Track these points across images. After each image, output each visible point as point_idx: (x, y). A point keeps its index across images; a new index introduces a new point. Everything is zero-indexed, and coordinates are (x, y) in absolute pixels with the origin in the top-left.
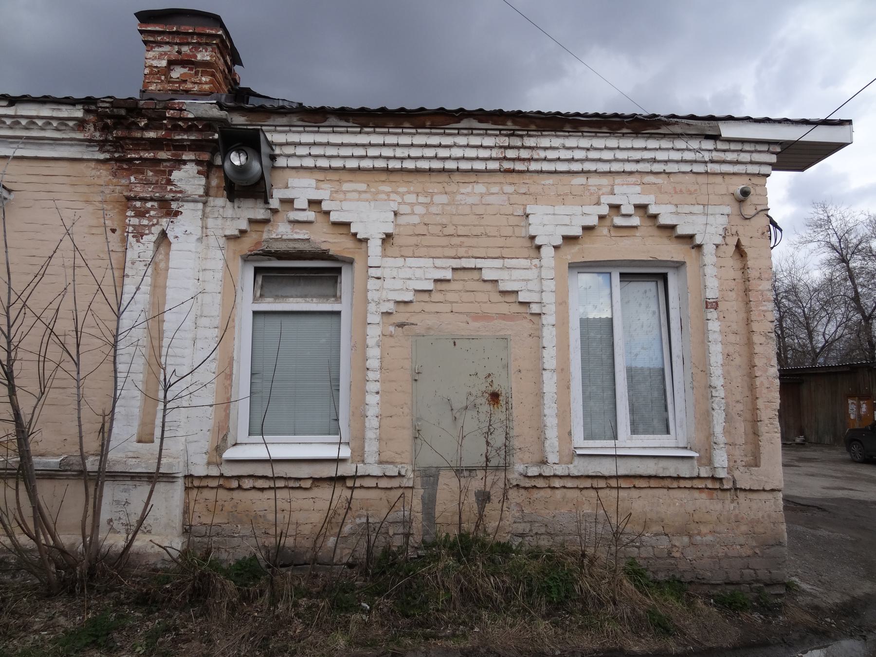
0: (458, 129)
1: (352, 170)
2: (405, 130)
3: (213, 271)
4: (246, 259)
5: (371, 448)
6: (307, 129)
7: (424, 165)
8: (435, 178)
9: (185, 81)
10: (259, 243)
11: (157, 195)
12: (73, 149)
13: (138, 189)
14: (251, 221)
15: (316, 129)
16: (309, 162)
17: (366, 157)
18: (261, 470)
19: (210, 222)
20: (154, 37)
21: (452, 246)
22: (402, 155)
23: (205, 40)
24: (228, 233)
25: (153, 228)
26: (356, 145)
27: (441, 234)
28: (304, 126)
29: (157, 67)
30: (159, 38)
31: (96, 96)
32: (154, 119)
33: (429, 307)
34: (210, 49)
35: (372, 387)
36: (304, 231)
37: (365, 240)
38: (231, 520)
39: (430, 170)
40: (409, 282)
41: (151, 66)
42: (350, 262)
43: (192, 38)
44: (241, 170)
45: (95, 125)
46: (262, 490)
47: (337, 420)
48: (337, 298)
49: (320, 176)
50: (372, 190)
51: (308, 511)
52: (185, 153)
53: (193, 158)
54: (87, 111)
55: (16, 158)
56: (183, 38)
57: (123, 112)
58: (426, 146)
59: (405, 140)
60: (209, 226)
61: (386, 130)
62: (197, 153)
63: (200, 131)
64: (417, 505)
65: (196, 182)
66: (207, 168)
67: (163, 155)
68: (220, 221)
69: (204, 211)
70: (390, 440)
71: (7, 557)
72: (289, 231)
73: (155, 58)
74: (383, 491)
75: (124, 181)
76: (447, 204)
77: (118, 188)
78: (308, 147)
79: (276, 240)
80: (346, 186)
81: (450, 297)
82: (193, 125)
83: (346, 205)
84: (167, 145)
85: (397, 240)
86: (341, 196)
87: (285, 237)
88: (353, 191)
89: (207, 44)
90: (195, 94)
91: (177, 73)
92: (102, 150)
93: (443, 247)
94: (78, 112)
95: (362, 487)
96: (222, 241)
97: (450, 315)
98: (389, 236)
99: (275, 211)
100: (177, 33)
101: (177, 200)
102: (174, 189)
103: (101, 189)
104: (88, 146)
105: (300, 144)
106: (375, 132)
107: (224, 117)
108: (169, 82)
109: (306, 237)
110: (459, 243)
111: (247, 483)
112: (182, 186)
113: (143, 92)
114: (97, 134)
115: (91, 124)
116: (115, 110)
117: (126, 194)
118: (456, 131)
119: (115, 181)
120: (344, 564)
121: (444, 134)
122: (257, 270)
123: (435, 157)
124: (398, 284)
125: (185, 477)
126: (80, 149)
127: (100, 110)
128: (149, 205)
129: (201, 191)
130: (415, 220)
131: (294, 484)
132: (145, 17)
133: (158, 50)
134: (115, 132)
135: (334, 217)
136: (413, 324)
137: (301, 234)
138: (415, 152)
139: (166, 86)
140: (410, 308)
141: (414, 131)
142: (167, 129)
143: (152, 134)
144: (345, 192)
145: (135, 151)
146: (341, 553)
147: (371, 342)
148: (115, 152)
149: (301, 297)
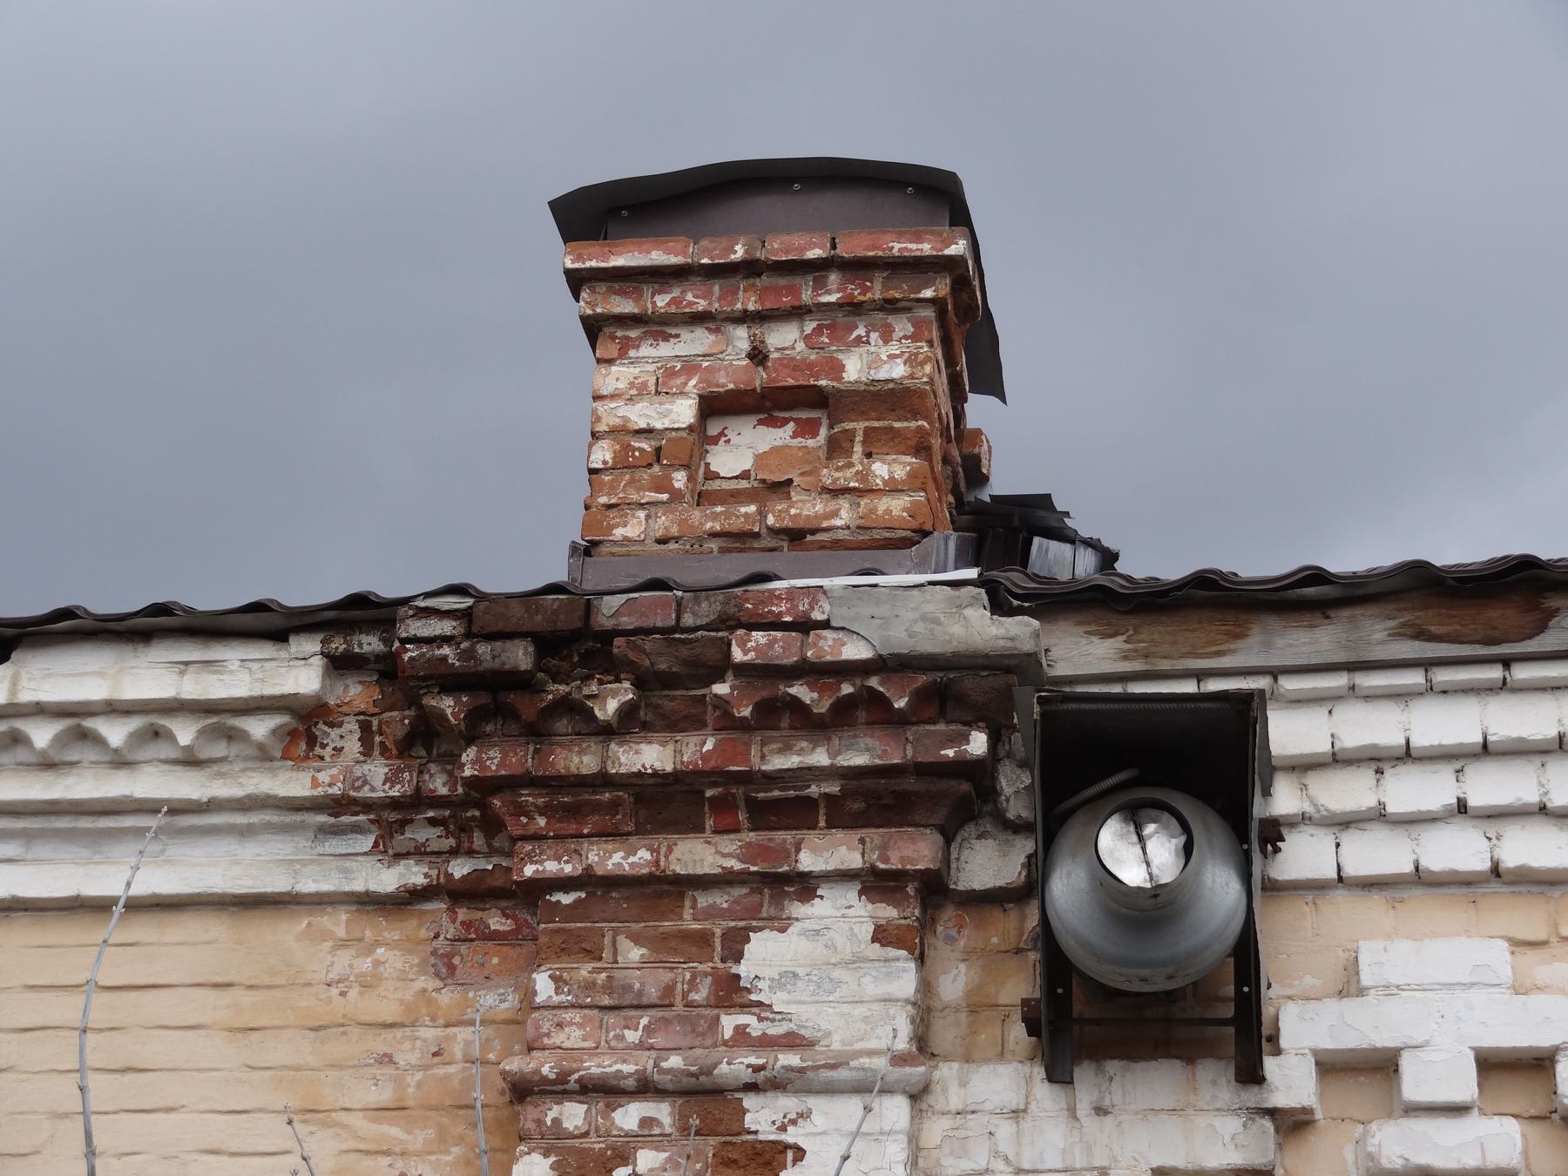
6: (1443, 676)
9: (781, 488)
11: (675, 1061)
12: (251, 851)
13: (572, 1037)
15: (1494, 673)
16: (1460, 850)
20: (638, 299)
23: (875, 289)
28: (1427, 664)
29: (648, 432)
30: (662, 301)
31: (388, 590)
32: (668, 681)
34: (902, 326)
41: (621, 432)
43: (820, 285)
44: (1151, 911)
45: (365, 728)
49: (1529, 918)
52: (812, 837)
53: (854, 860)
54: (339, 665)
55: (142, 906)
57: (520, 656)
62: (875, 835)
63: (894, 721)
65: (872, 986)
66: (922, 906)
67: (697, 854)
69: (914, 1140)
73: (638, 392)
75: (496, 1000)
82: (859, 697)
84: (723, 806)
89: (890, 306)
90: (837, 545)
91: (740, 450)
94: (298, 673)
99: (1292, 1124)
100: (750, 268)
101: (776, 1084)
102: (756, 1028)
103: (380, 1043)
104: (325, 831)
105: (1407, 755)
107: (1027, 646)
108: (702, 498)
112: (797, 1008)
113: (586, 550)
114: (377, 771)
115: (351, 725)
116: (483, 649)
117: (514, 1065)
119: (446, 998)
126: (282, 847)
127: (412, 652)
128: (629, 1116)
129: (898, 1032)
132: (588, 214)
133: (653, 353)
134: (469, 755)
139: (696, 515)
142: (728, 722)
143: (649, 756)
148: (454, 852)
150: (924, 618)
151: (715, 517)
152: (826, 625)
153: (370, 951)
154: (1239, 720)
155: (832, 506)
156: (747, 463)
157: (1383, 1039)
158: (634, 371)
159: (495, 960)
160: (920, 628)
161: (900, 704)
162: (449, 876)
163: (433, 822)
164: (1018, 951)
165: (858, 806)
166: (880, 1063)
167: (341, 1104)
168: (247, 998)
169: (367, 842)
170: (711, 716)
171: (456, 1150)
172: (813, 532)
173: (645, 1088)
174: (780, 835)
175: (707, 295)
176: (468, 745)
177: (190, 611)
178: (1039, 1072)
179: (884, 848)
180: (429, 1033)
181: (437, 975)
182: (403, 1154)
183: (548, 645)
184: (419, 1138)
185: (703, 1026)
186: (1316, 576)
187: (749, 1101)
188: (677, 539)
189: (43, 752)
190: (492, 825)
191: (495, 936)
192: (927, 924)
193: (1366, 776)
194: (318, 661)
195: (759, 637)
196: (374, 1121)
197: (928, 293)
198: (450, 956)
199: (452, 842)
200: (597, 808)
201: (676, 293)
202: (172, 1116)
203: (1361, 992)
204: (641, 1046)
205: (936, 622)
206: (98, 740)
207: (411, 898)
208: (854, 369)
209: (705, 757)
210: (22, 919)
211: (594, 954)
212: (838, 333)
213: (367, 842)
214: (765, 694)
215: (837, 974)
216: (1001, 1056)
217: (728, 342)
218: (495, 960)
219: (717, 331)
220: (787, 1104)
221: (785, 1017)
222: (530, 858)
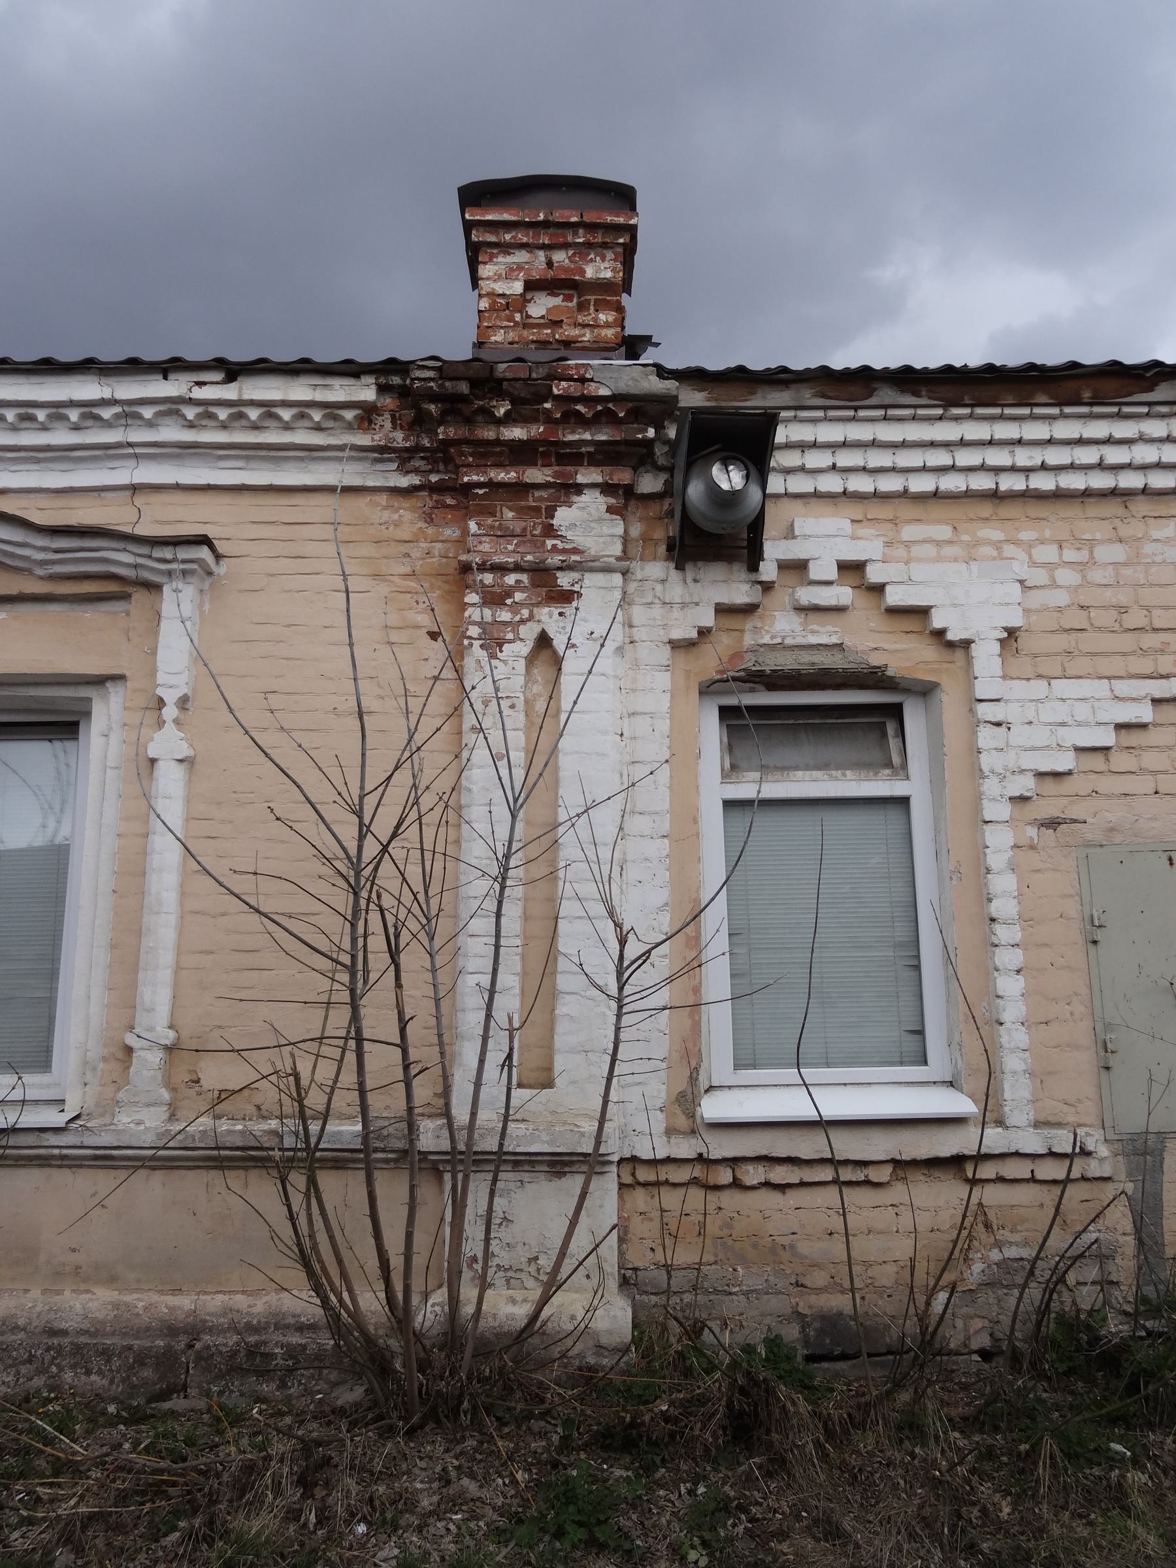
0: (1149, 404)
1: (921, 497)
2: (1037, 410)
3: (652, 715)
4: (706, 690)
5: (1016, 1093)
6: (831, 413)
7: (1074, 482)
8: (1095, 509)
10: (737, 655)
11: (529, 558)
14: (722, 610)
15: (851, 413)
16: (831, 484)
17: (953, 468)
18: (782, 1145)
19: (638, 613)
20: (497, 234)
21: (1144, 652)
22: (1029, 463)
24: (677, 634)
25: (522, 629)
26: (932, 444)
27: (1117, 627)
28: (825, 408)
29: (503, 295)
30: (508, 237)
31: (404, 357)
33: (1107, 784)
34: (610, 255)
35: (1008, 958)
36: (830, 628)
37: (966, 644)
38: (721, 1256)
39: (1087, 493)
40: (1062, 731)
41: (492, 295)
42: (926, 691)
43: (575, 234)
44: (732, 499)
45: (393, 417)
46: (783, 1188)
47: (920, 1033)
48: (902, 770)
49: (857, 511)
50: (965, 538)
51: (898, 1229)
52: (582, 469)
53: (599, 479)
54: (382, 389)
56: (555, 232)
57: (464, 388)
58: (1081, 442)
59: (1038, 431)
60: (635, 622)
61: (998, 411)
62: (607, 469)
64: (1120, 1219)
66: (624, 498)
67: (535, 475)
68: (657, 611)
70: (1049, 1073)
71: (265, 1343)
72: (798, 628)
74: (1045, 1188)
75: (452, 532)
76: (1125, 564)
77: (439, 545)
78: (828, 452)
79: (772, 647)
80: (909, 532)
81: (1151, 760)
82: (605, 411)
83: (918, 571)
84: (546, 455)
85: (1024, 641)
86: (900, 552)
87: (789, 641)
88: (924, 541)
89: (605, 246)
90: (584, 349)
91: (541, 306)
92: (403, 470)
93: (1124, 654)
94: (365, 391)
95: (1001, 1179)
96: (665, 654)
97: (1155, 799)
98: (1012, 632)
99: (767, 587)
100: (546, 224)
102: (560, 545)
104: (377, 461)
105: (814, 445)
106: (971, 417)
108: (526, 326)
109: (834, 640)
110: (1158, 646)
111: (753, 1175)
112: (577, 538)
113: (479, 345)
114: (399, 436)
115: (387, 416)
116: (447, 384)
118: (1145, 410)
119: (430, 531)
120: (975, 1352)
121: (1120, 416)
122: (727, 713)
123: (1101, 466)
124: (1041, 736)
125: (621, 1161)
126: (358, 467)
128: (511, 579)
130: (1061, 598)
131: (848, 1174)
132: (475, 195)
134: (441, 430)
135: (895, 597)
136: (1075, 821)
137: (824, 633)
138: (1055, 456)
139: (525, 333)
140: (1068, 786)
141: (1055, 411)
142: (549, 419)
143: (517, 433)
144: (908, 545)
145: (479, 467)
146: (966, 1328)
147: (997, 860)
148: (431, 471)
149: (817, 767)
150: (632, 379)
151: (534, 334)
152: (591, 380)
153: (397, 511)
154: (769, 421)
155: (583, 332)
156: (544, 312)
157: (803, 556)
158: (496, 268)
160: (630, 383)
161: (622, 415)
163: (422, 458)
164: (660, 518)
165: (600, 457)
166: (612, 560)
169: (394, 466)
170: (542, 417)
172: (575, 342)
173: (517, 568)
174: (569, 468)
175: (527, 235)
176: (439, 426)
178: (672, 565)
179: (611, 475)
180: (424, 545)
183: (474, 383)
185: (539, 544)
186: (784, 370)
187: (559, 574)
188: (517, 343)
189: (254, 422)
190: (448, 460)
191: (449, 506)
192: (626, 506)
193: (798, 453)
194: (374, 387)
195: (564, 384)
197: (621, 241)
198: (431, 514)
200: (494, 454)
201: (514, 233)
203: (794, 537)
204: (514, 551)
205: (637, 381)
206: (277, 417)
207: (411, 491)
208: (590, 272)
209: (540, 434)
210: (247, 494)
211: (493, 515)
212: (583, 256)
213: (394, 466)
214: (565, 408)
215: (593, 525)
216: (655, 559)
217: (536, 257)
219: (531, 252)
220: (575, 575)
221: (572, 541)
222: (466, 474)
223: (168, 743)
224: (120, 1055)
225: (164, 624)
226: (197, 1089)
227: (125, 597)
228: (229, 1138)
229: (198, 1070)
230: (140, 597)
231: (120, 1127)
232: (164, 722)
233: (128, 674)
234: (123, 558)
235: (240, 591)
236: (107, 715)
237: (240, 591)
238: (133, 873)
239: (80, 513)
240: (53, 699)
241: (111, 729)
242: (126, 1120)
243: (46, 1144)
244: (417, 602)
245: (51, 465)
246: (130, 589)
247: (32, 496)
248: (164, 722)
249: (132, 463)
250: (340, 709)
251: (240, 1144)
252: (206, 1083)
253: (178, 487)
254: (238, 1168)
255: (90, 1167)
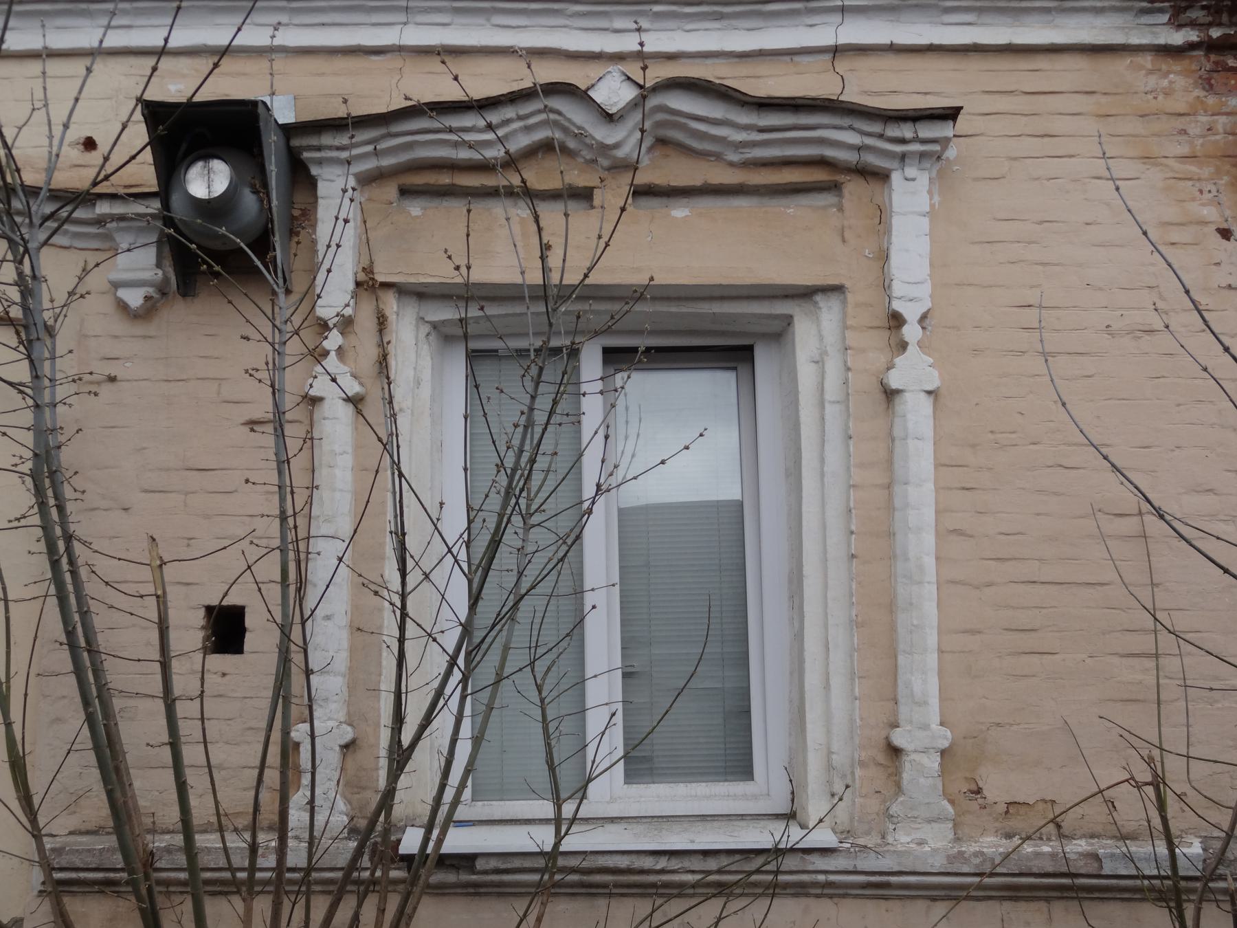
103: (1179, 123)
119: (1211, 100)
148: (1210, 25)
153: (1166, 75)
159: (1233, 82)
162: (1210, 37)
163: (1203, 8)
167: (1163, 154)
168: (1103, 99)
169: (1165, 18)
171: (1225, 178)
177: (38, 259)
181: (1204, 89)
182: (1199, 180)
184: (1206, 172)
196: (1181, 163)
198: (1209, 80)
199: (1210, 19)
202: (1073, 159)
207: (1192, 46)
213: (1165, 18)
218: (1233, 82)
223: (913, 371)
224: (881, 758)
225: (896, 222)
226: (980, 801)
227: (835, 187)
228: (1036, 862)
229: (978, 779)
230: (853, 188)
231: (900, 848)
232: (907, 344)
233: (848, 284)
234: (845, 139)
235: (976, 179)
236: (815, 335)
237: (976, 179)
238: (876, 534)
239: (771, 82)
240: (734, 318)
241: (826, 353)
242: (904, 839)
243: (811, 868)
244: (1201, 192)
245: (735, 23)
246: (841, 178)
247: (709, 61)
248: (907, 344)
249: (837, 18)
250: (1114, 327)
251: (1050, 869)
252: (991, 793)
253: (893, 49)
254: (1038, 899)
255: (856, 896)
